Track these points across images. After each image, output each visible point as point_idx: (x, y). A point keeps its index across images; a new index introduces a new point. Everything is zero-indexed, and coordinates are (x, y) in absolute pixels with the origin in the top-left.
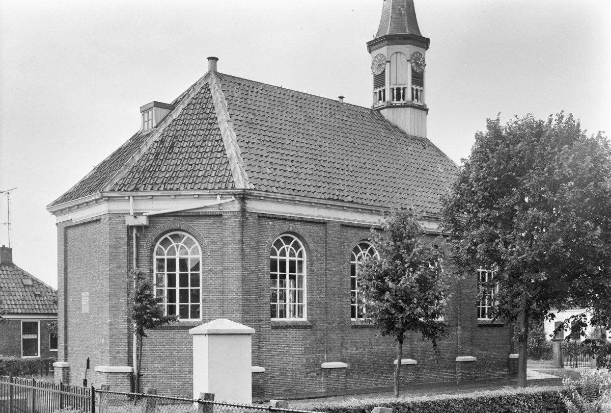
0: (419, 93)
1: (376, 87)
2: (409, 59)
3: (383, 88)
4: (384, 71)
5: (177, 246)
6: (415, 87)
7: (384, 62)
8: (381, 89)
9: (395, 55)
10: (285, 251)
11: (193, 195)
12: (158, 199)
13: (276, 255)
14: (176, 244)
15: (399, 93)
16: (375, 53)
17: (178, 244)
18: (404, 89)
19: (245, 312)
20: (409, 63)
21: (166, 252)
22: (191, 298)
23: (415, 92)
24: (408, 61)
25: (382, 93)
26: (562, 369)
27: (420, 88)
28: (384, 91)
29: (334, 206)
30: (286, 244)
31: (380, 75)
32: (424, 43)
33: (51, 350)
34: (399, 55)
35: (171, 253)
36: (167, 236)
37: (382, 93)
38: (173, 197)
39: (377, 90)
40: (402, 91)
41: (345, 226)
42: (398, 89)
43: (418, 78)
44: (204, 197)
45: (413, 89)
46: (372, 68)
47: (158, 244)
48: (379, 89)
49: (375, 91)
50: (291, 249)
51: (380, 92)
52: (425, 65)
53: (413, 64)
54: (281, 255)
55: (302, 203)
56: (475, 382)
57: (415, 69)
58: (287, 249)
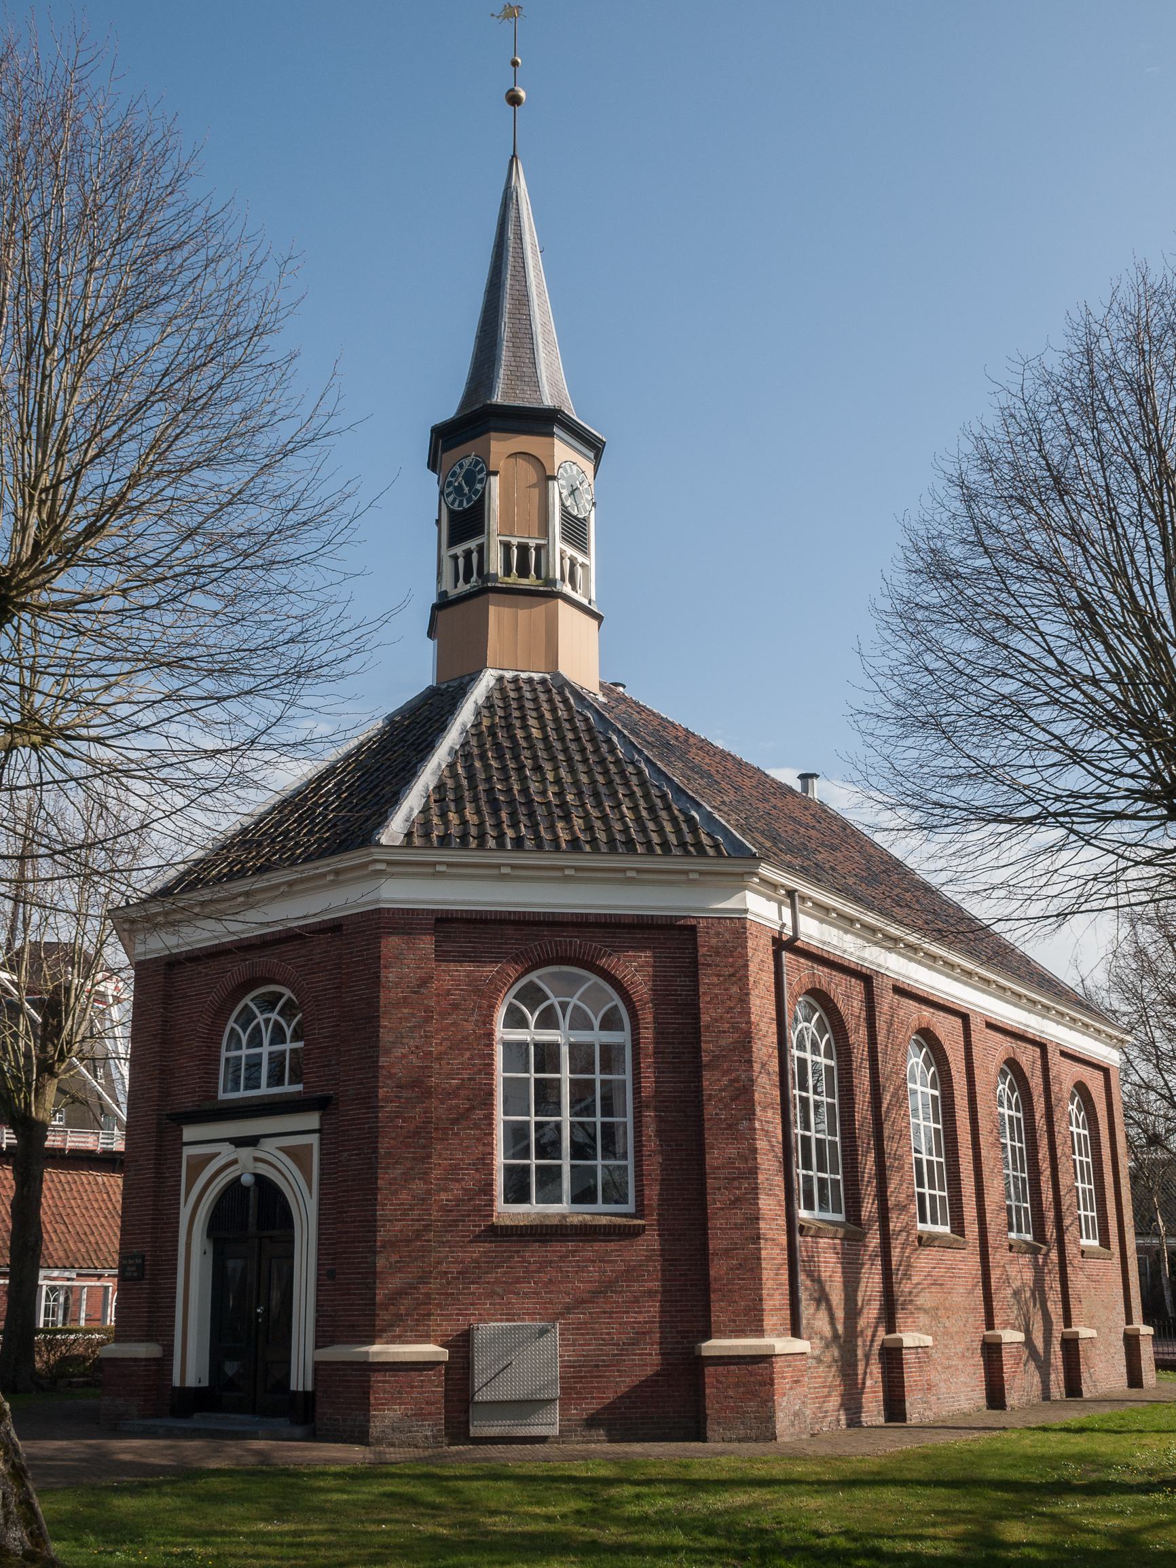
1: (453, 542)
3: (479, 542)
5: (564, 1006)
8: (472, 544)
10: (260, 1031)
12: (351, 880)
17: (567, 999)
19: (554, 1180)
22: (603, 1139)
25: (475, 556)
26: (451, 1328)
28: (481, 549)
29: (302, 881)
35: (233, 1046)
37: (475, 556)
38: (330, 877)
39: (459, 550)
47: (617, 1001)
50: (277, 1023)
51: (468, 554)
55: (312, 885)
56: (468, 1368)
57: (568, 504)
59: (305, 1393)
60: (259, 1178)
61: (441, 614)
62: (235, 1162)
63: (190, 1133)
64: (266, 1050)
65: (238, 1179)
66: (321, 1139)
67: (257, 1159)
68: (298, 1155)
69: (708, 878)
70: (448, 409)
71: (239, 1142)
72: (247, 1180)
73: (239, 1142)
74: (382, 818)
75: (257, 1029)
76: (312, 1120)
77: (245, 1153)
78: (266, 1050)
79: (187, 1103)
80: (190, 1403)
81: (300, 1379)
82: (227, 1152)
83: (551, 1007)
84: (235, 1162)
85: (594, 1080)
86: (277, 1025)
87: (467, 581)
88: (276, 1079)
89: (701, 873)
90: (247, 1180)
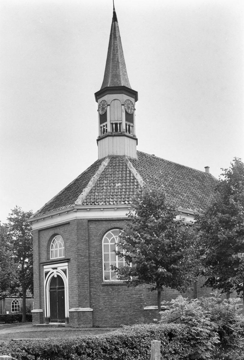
0: (131, 127)
2: (123, 103)
4: (106, 112)
6: (128, 123)
7: (106, 105)
8: (105, 124)
9: (113, 101)
11: (114, 208)
13: (108, 242)
14: (116, 236)
15: (116, 126)
16: (100, 100)
18: (120, 124)
20: (123, 106)
21: (110, 241)
23: (128, 126)
24: (122, 105)
27: (131, 124)
30: (115, 235)
31: (103, 114)
32: (134, 94)
33: (12, 312)
34: (116, 101)
36: (110, 232)
39: (102, 125)
40: (118, 125)
41: (90, 221)
42: (116, 124)
43: (130, 117)
44: (93, 210)
45: (126, 125)
46: (98, 110)
48: (103, 125)
49: (101, 126)
50: (60, 243)
52: (135, 109)
53: (126, 108)
54: (111, 242)
55: (121, 209)
57: (127, 111)
58: (58, 244)
59: (68, 318)
60: (58, 275)
61: (99, 142)
62: (53, 273)
63: (45, 267)
64: (58, 249)
65: (54, 276)
66: (68, 268)
67: (57, 272)
68: (65, 271)
69: (119, 209)
70: (98, 88)
71: (54, 269)
72: (56, 276)
73: (54, 269)
74: (76, 196)
75: (57, 244)
76: (66, 264)
77: (55, 271)
78: (58, 249)
79: (44, 260)
80: (49, 320)
81: (67, 315)
82: (52, 271)
83: (114, 238)
84: (53, 273)
85: (111, 252)
86: (60, 244)
87: (104, 133)
88: (60, 255)
89: (103, 208)
90: (56, 276)
